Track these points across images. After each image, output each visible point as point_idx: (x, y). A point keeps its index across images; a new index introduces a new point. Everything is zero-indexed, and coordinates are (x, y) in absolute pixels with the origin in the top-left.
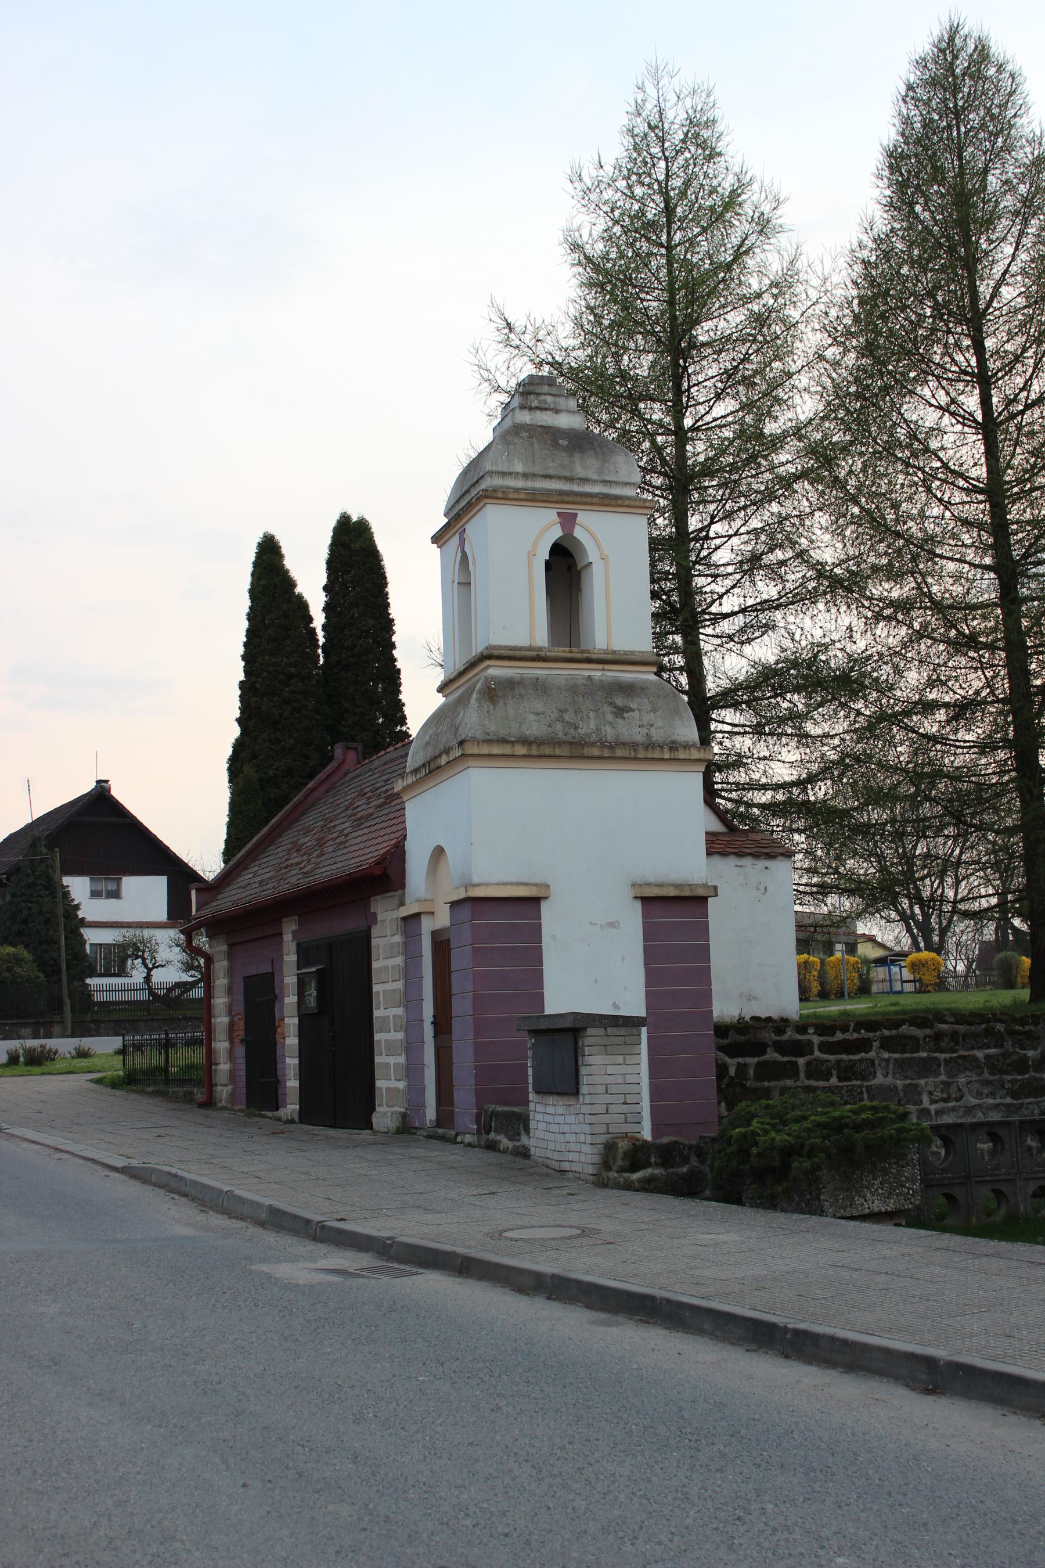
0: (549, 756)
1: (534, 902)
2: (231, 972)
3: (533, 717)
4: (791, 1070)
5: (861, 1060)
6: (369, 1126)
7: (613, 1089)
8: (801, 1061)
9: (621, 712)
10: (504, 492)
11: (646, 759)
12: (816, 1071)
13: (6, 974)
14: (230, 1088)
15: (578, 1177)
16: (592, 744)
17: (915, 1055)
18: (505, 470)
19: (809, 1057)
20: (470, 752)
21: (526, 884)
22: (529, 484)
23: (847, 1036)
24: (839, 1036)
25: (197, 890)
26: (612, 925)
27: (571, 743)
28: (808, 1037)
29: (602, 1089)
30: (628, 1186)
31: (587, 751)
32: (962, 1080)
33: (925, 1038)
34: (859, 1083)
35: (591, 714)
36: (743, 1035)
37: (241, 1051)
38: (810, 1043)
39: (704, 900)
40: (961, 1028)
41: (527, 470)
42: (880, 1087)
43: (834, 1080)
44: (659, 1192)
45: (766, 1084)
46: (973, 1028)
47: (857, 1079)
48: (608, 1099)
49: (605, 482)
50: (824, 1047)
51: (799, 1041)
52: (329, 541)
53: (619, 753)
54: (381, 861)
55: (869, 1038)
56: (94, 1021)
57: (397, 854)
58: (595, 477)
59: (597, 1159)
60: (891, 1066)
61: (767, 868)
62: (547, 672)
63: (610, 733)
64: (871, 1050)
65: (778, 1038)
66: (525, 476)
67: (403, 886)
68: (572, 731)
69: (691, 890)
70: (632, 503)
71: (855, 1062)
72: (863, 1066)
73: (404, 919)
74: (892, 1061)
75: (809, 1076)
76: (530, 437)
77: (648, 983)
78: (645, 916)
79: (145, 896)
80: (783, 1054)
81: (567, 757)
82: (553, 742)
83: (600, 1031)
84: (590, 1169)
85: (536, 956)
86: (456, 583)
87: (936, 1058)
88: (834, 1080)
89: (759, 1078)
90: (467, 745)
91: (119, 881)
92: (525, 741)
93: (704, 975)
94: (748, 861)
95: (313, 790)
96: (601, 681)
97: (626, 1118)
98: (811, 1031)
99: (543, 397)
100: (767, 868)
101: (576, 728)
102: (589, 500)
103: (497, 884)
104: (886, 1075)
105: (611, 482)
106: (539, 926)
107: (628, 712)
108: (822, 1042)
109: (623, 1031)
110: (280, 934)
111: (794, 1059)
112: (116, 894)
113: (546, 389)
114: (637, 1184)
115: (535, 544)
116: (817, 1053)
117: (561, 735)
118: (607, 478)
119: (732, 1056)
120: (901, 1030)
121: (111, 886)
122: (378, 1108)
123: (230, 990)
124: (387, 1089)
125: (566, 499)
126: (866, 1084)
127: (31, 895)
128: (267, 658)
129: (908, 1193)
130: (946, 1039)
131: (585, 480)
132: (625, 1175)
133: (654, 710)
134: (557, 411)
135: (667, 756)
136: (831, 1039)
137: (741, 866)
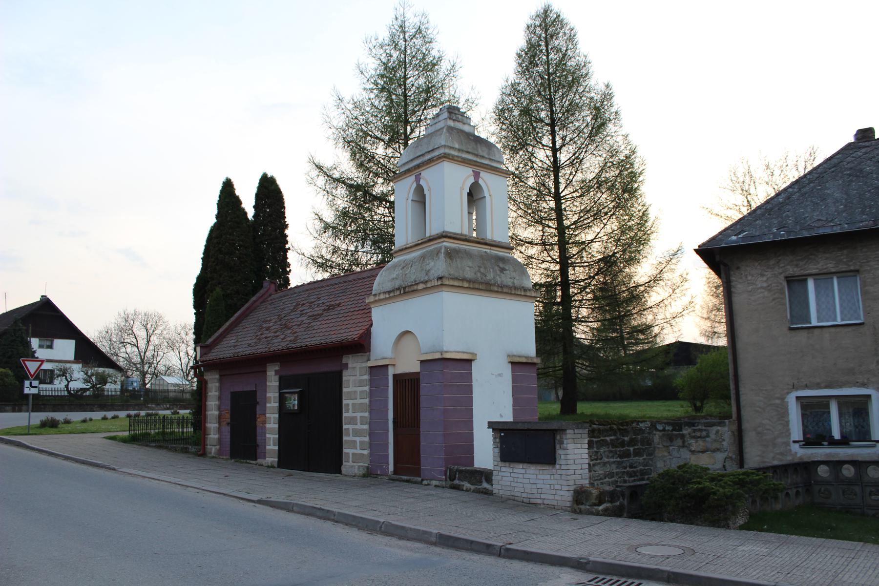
1: (469, 361)
2: (221, 389)
6: (340, 472)
14: (218, 447)
15: (551, 508)
16: (494, 285)
22: (460, 154)
29: (572, 462)
30: (597, 514)
32: (602, 450)
37: (227, 430)
40: (601, 427)
48: (575, 467)
49: (490, 159)
52: (257, 185)
54: (361, 336)
56: (43, 404)
57: (367, 335)
59: (570, 499)
66: (459, 150)
67: (369, 351)
73: (370, 367)
79: (65, 349)
84: (568, 504)
86: (410, 201)
90: (444, 280)
91: (52, 342)
95: (255, 302)
110: (265, 371)
112: (50, 347)
121: (48, 343)
122: (344, 463)
124: (353, 454)
131: (483, 157)
133: (515, 271)
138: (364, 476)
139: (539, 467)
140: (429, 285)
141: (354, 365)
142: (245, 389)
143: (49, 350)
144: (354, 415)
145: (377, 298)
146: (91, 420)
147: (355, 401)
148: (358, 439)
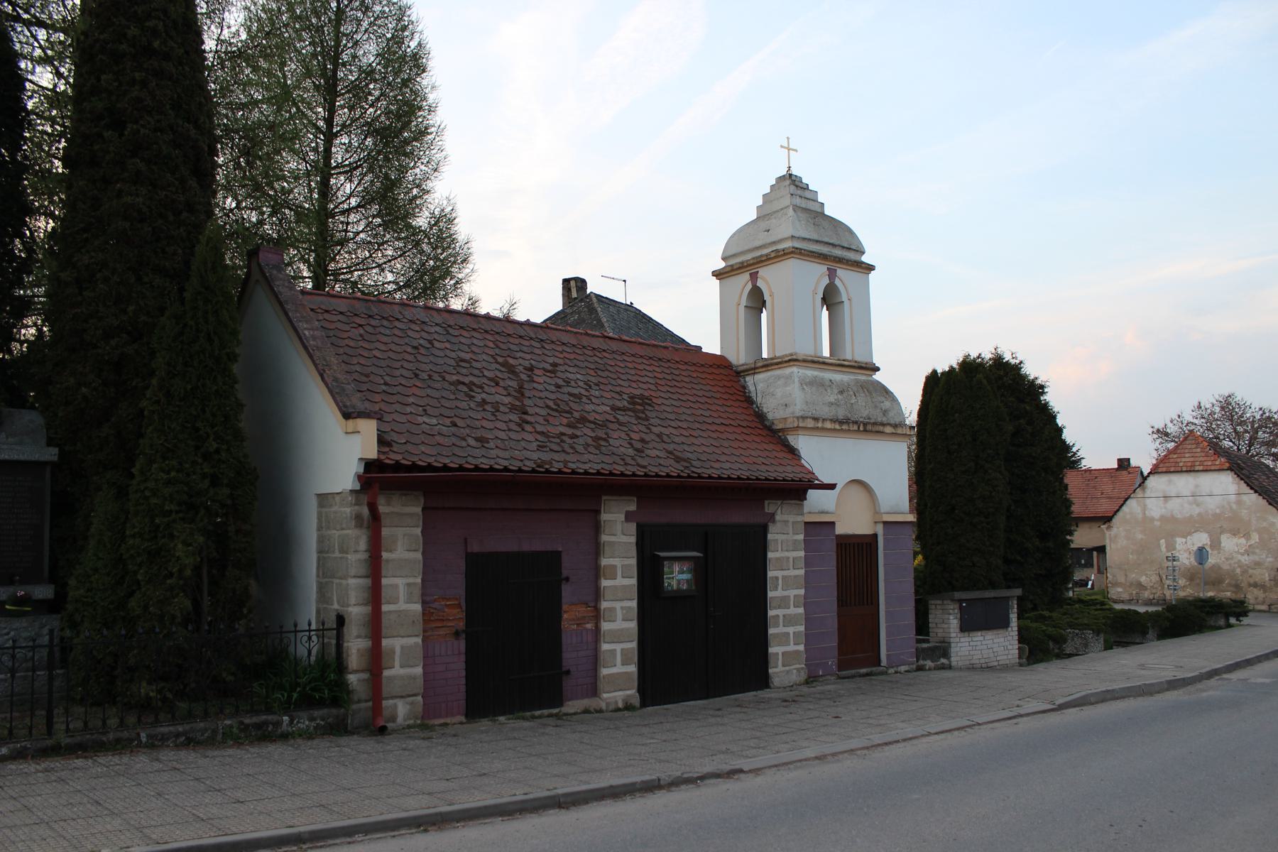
15: (1005, 668)
110: (598, 512)
138: (807, 682)
139: (995, 632)
140: (899, 431)
141: (785, 517)
142: (526, 547)
144: (786, 593)
145: (820, 425)
147: (785, 573)
148: (791, 630)
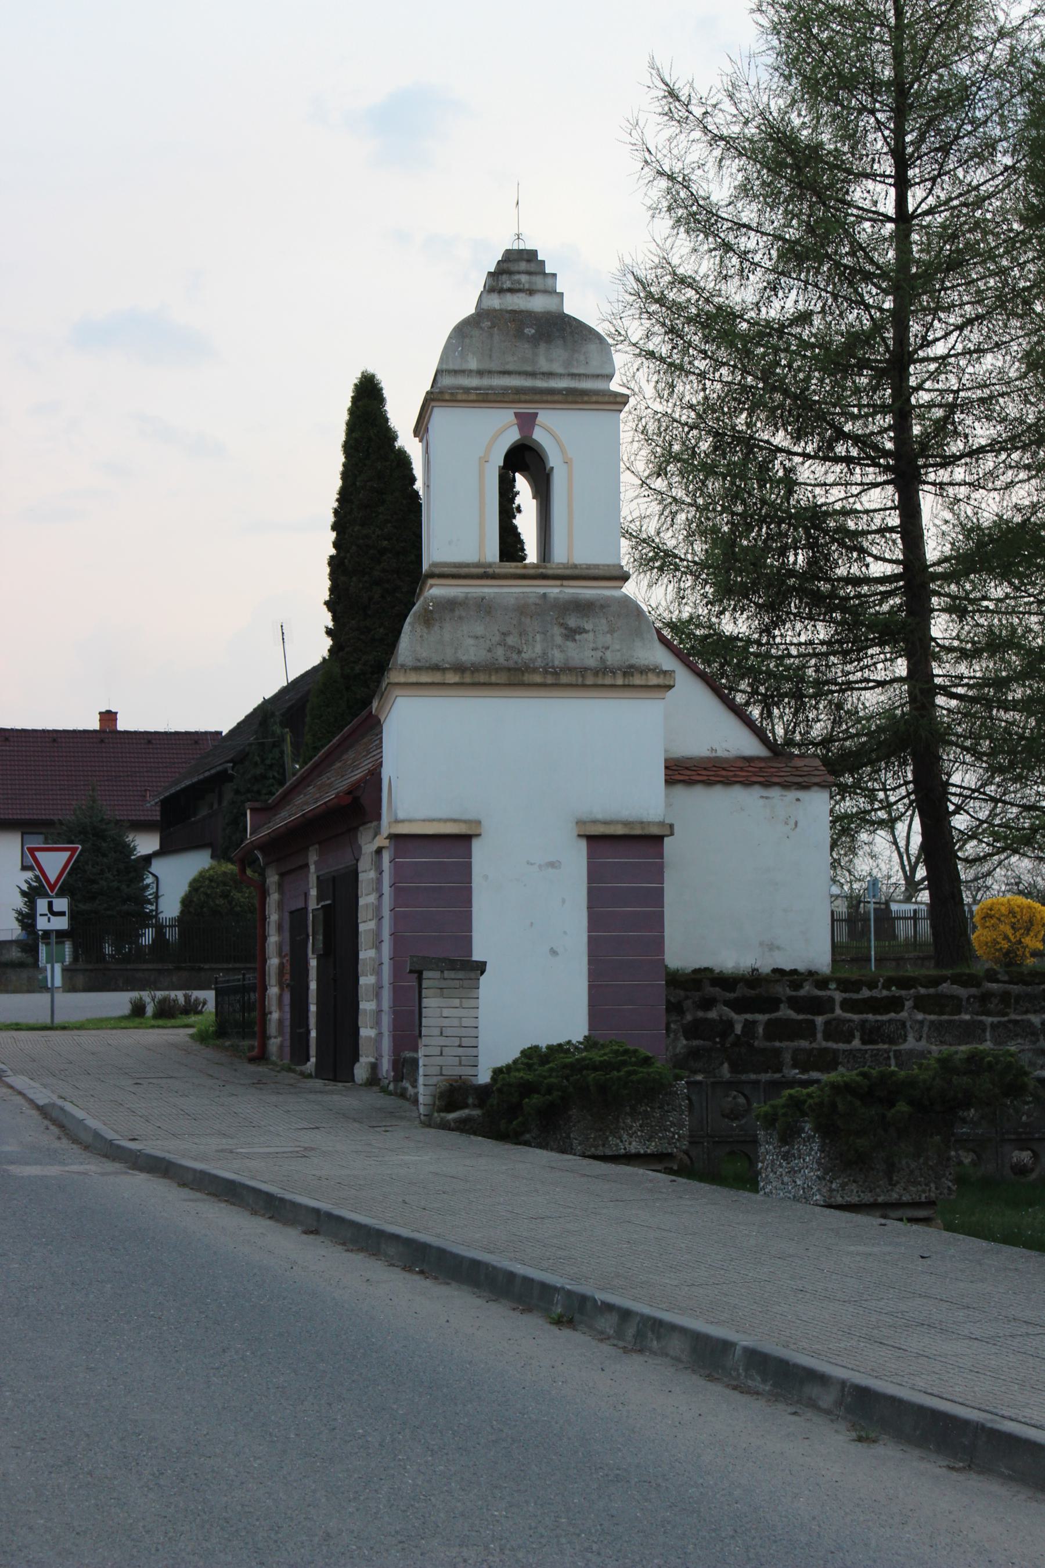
0: (484, 684)
1: (464, 840)
3: (471, 641)
4: (807, 1030)
5: (890, 1021)
7: (448, 1032)
8: (820, 1020)
9: (572, 633)
10: (452, 394)
11: (595, 686)
12: (836, 1031)
13: (220, 901)
16: (535, 670)
17: (956, 1017)
18: (456, 368)
19: (829, 1016)
20: (396, 680)
21: (455, 821)
22: (486, 382)
23: (875, 993)
24: (865, 993)
25: (252, 810)
26: (552, 865)
27: (509, 669)
28: (829, 993)
29: (437, 1032)
30: (444, 1126)
31: (527, 678)
33: (968, 999)
34: (886, 1046)
35: (538, 637)
36: (753, 988)
38: (831, 1000)
39: (659, 839)
41: (482, 367)
42: (911, 1052)
43: (856, 1043)
44: (475, 1134)
45: (777, 1044)
46: (1029, 989)
47: (884, 1043)
48: (442, 1041)
49: (573, 376)
50: (846, 1005)
51: (818, 997)
53: (564, 679)
55: (900, 997)
58: (561, 370)
60: (925, 1029)
61: (798, 800)
62: (496, 590)
63: (558, 658)
64: (902, 1010)
65: (794, 993)
66: (480, 373)
68: (515, 656)
69: (643, 828)
70: (600, 399)
71: (883, 1023)
72: (892, 1028)
74: (927, 1024)
75: (827, 1037)
76: (492, 327)
77: (590, 929)
78: (590, 856)
80: (799, 1011)
81: (505, 685)
82: (492, 668)
83: (437, 974)
85: (464, 896)
87: (981, 1022)
88: (856, 1043)
89: (769, 1036)
92: (459, 668)
93: (657, 921)
94: (775, 793)
96: (556, 599)
97: (460, 1061)
98: (833, 986)
99: (517, 277)
100: (798, 800)
101: (519, 652)
102: (549, 398)
103: (424, 821)
104: (919, 1039)
105: (579, 375)
106: (469, 866)
107: (580, 633)
108: (845, 999)
109: (461, 975)
111: (810, 1017)
113: (523, 266)
114: (452, 1124)
115: (488, 449)
116: (838, 1011)
117: (502, 660)
118: (575, 371)
119: (739, 1012)
120: (940, 988)
123: (280, 928)
125: (523, 397)
126: (894, 1048)
127: (259, 792)
128: (357, 528)
129: (673, 1138)
130: (995, 1001)
131: (550, 375)
132: (443, 1114)
133: (612, 631)
134: (531, 292)
135: (620, 682)
136: (855, 996)
137: (767, 798)
143: (676, 828)
146: (1012, 1083)
